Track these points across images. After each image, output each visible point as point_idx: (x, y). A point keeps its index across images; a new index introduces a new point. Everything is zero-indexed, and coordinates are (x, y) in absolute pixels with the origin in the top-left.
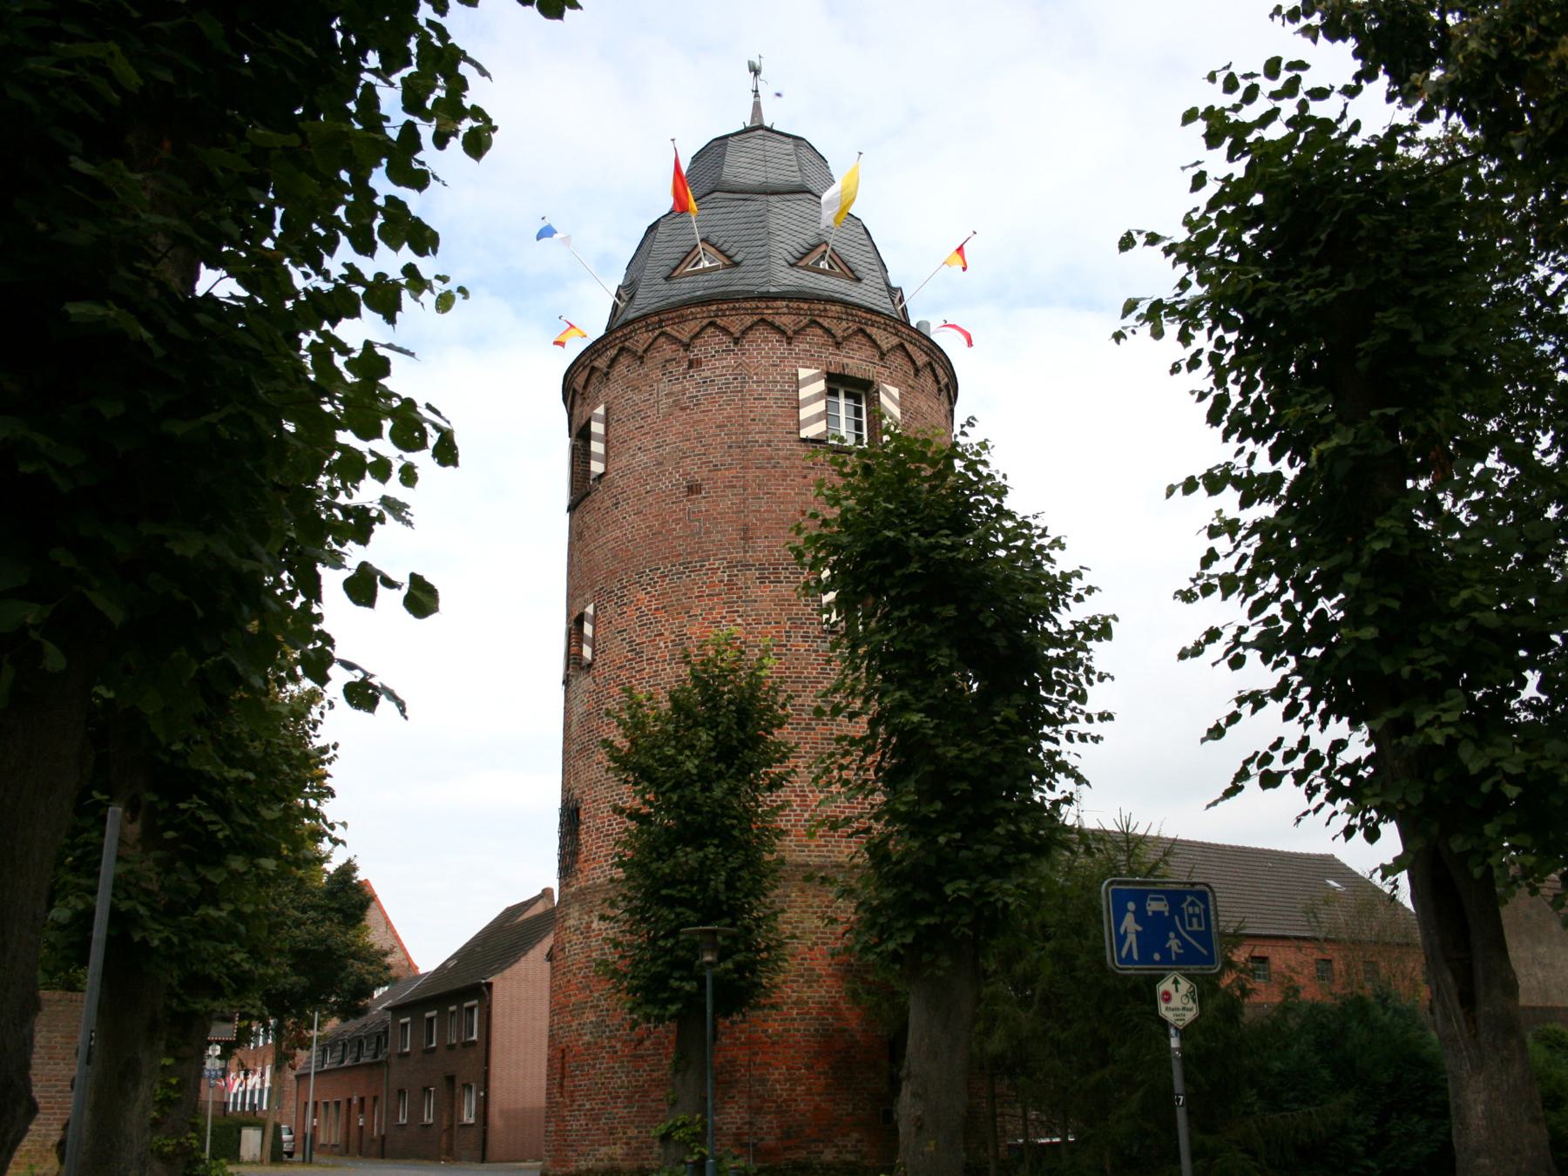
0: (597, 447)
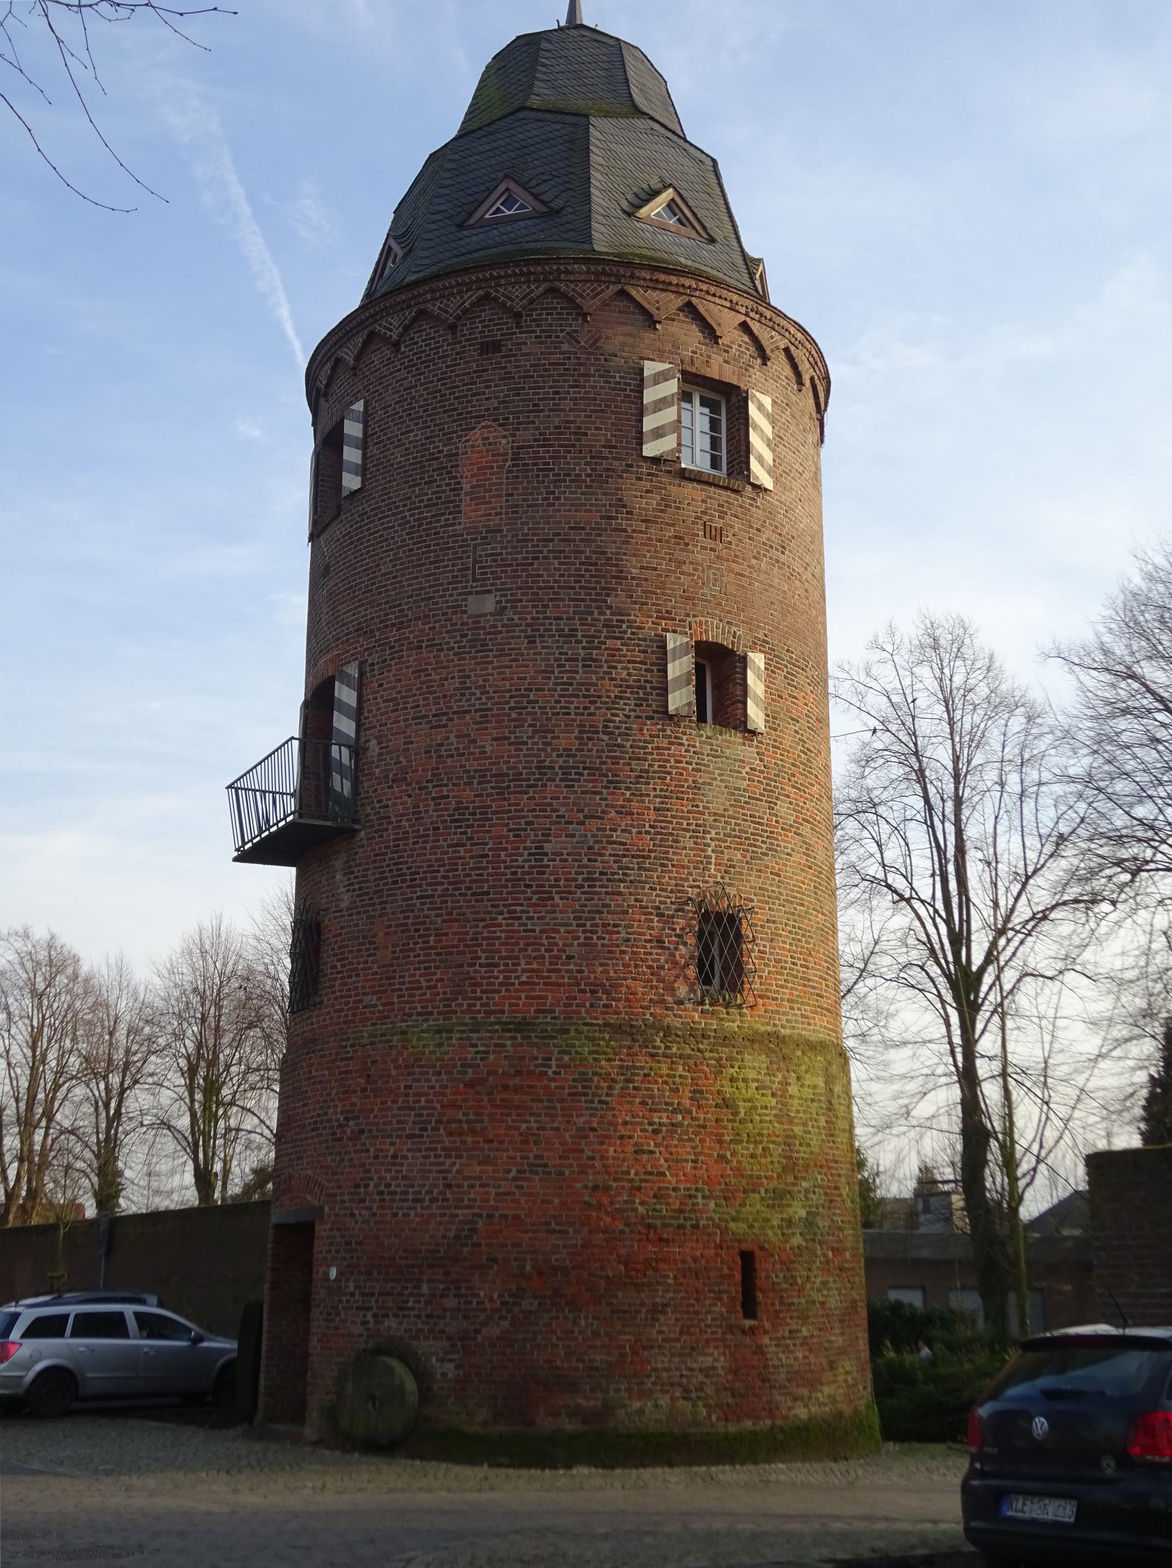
0: (352, 455)
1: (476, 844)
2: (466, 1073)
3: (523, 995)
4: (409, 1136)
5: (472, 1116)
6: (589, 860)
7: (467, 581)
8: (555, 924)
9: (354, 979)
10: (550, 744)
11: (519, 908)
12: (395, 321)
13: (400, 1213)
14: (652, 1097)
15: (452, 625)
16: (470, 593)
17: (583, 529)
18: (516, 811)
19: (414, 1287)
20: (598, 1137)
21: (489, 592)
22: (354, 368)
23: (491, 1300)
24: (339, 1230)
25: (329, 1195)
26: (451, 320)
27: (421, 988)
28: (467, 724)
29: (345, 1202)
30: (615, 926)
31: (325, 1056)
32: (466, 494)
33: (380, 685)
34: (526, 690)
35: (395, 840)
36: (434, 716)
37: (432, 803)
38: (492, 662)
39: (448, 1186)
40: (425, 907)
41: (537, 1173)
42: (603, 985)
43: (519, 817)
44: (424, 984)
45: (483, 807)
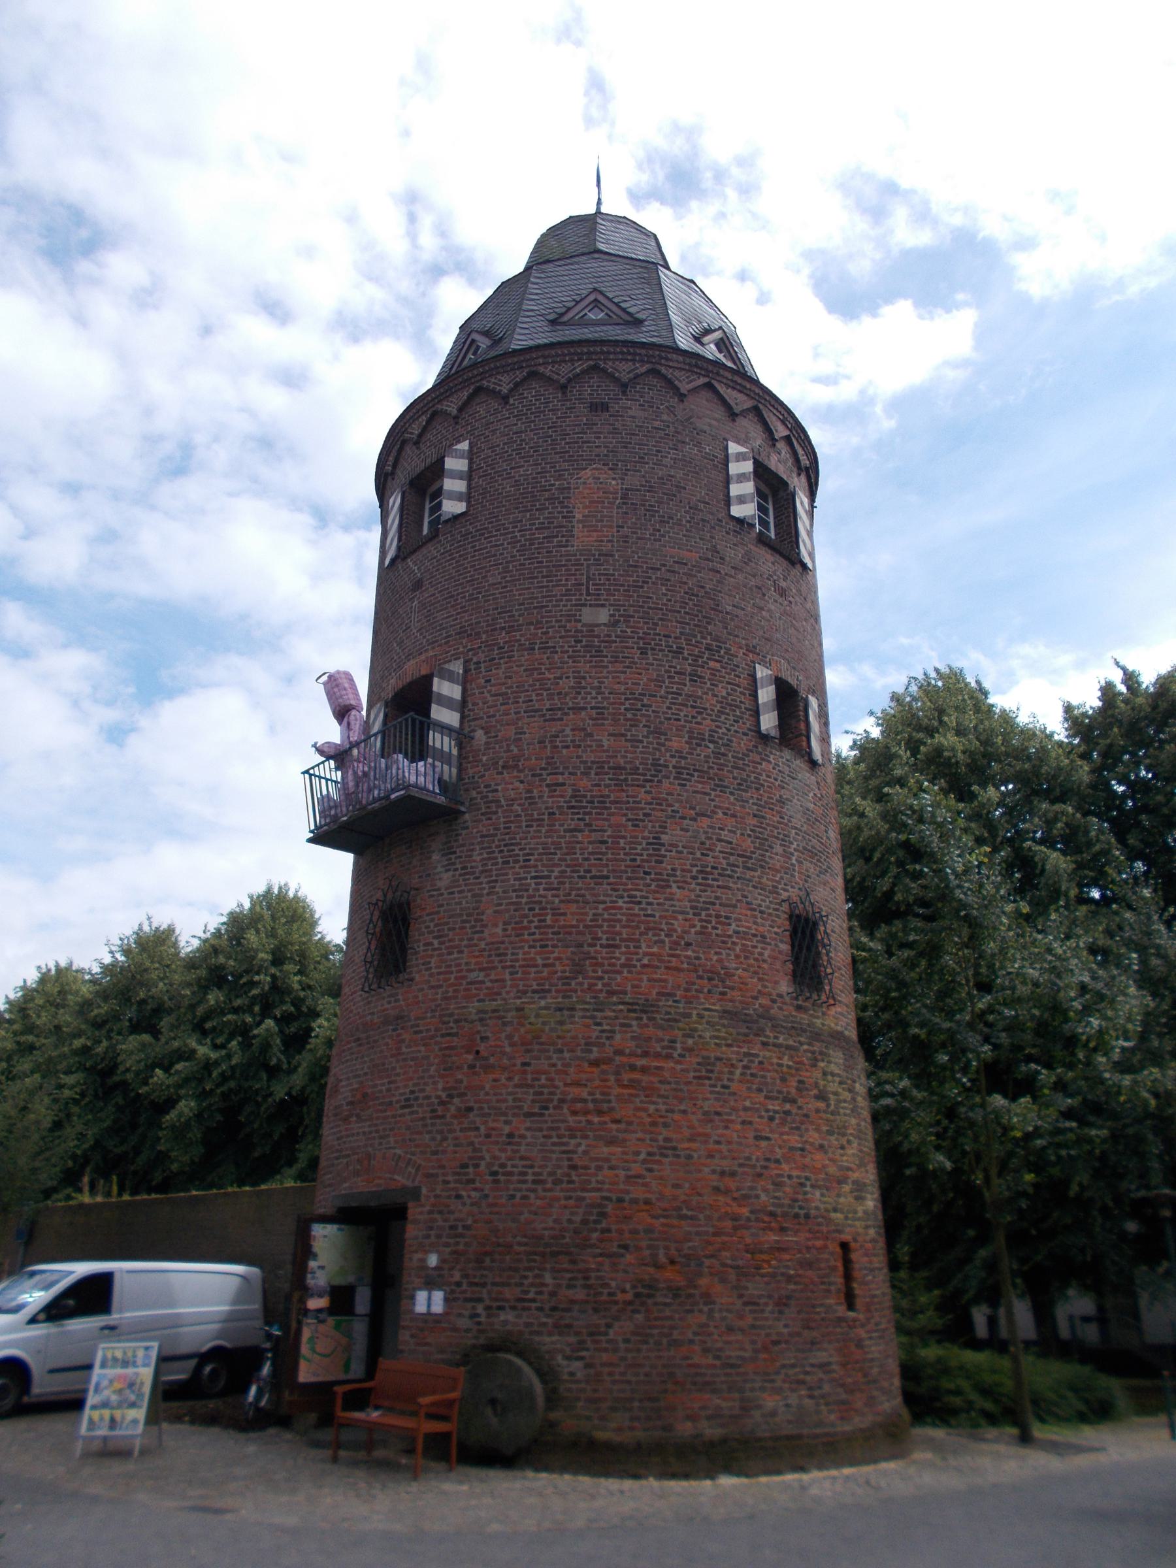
1: (595, 831)
2: (591, 1051)
3: (645, 977)
4: (529, 1115)
5: (598, 1096)
6: (703, 854)
7: (581, 595)
8: (673, 912)
9: (456, 955)
10: (664, 745)
11: (638, 893)
12: (505, 378)
13: (519, 1195)
14: (766, 1084)
15: (567, 631)
16: (585, 605)
17: (685, 564)
18: (634, 802)
19: (536, 1276)
20: (723, 1121)
21: (603, 605)
22: (456, 417)
23: (624, 1291)
24: (440, 1212)
25: (428, 1176)
26: (563, 381)
27: (536, 966)
28: (583, 720)
29: (448, 1182)
30: (727, 917)
31: (421, 1032)
32: (578, 522)
33: (488, 681)
34: (640, 694)
35: (505, 823)
36: (548, 710)
37: (546, 789)
38: (607, 667)
39: (574, 1167)
40: (541, 887)
41: (666, 1156)
42: (718, 974)
43: (637, 809)
44: (540, 961)
45: (602, 796)
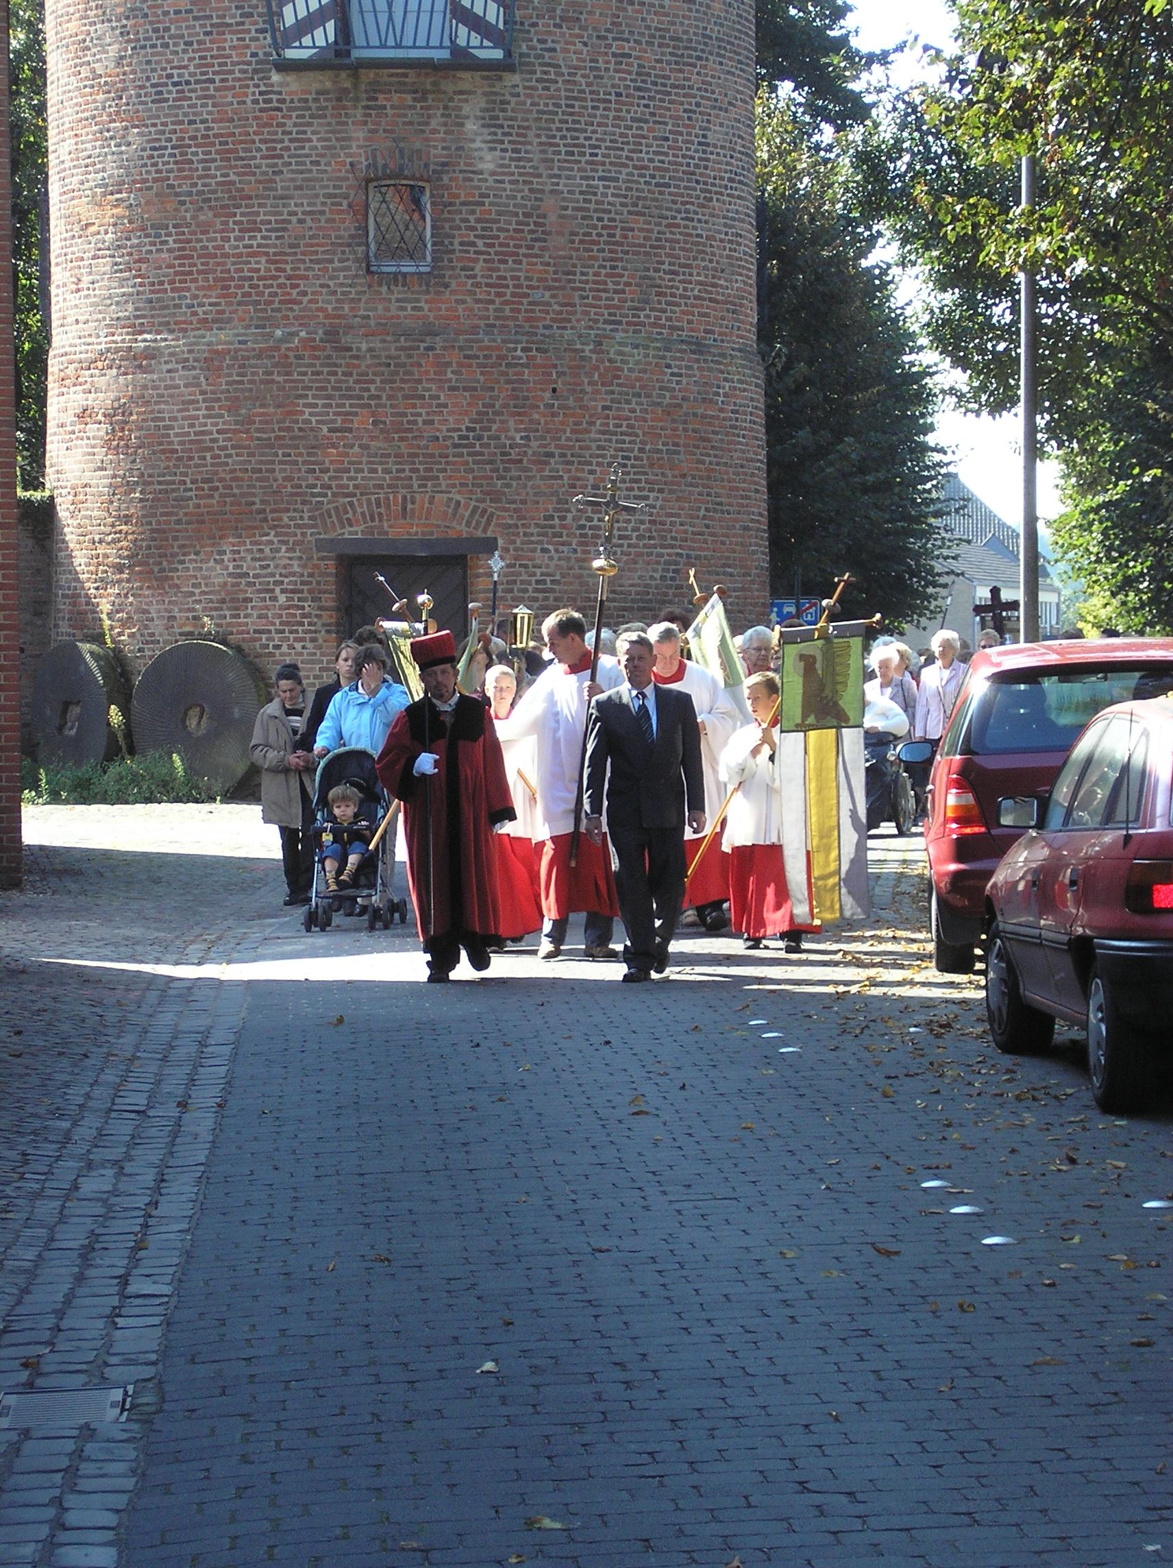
40: (609, 192)
